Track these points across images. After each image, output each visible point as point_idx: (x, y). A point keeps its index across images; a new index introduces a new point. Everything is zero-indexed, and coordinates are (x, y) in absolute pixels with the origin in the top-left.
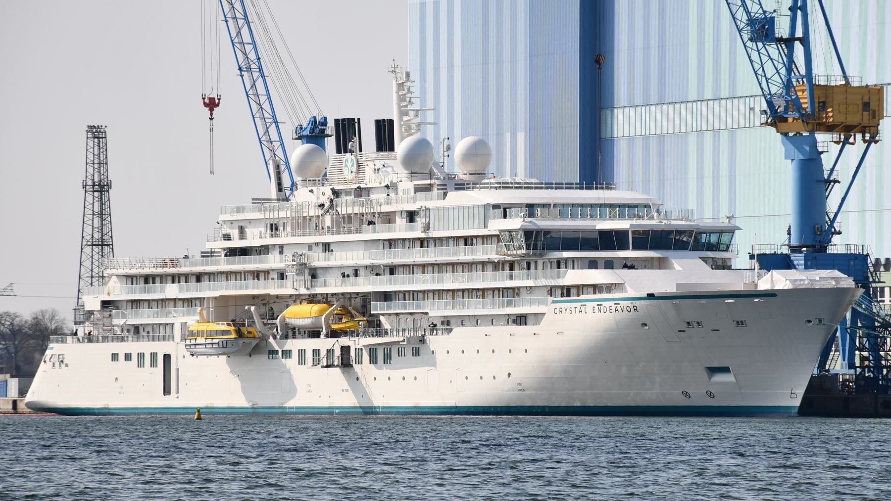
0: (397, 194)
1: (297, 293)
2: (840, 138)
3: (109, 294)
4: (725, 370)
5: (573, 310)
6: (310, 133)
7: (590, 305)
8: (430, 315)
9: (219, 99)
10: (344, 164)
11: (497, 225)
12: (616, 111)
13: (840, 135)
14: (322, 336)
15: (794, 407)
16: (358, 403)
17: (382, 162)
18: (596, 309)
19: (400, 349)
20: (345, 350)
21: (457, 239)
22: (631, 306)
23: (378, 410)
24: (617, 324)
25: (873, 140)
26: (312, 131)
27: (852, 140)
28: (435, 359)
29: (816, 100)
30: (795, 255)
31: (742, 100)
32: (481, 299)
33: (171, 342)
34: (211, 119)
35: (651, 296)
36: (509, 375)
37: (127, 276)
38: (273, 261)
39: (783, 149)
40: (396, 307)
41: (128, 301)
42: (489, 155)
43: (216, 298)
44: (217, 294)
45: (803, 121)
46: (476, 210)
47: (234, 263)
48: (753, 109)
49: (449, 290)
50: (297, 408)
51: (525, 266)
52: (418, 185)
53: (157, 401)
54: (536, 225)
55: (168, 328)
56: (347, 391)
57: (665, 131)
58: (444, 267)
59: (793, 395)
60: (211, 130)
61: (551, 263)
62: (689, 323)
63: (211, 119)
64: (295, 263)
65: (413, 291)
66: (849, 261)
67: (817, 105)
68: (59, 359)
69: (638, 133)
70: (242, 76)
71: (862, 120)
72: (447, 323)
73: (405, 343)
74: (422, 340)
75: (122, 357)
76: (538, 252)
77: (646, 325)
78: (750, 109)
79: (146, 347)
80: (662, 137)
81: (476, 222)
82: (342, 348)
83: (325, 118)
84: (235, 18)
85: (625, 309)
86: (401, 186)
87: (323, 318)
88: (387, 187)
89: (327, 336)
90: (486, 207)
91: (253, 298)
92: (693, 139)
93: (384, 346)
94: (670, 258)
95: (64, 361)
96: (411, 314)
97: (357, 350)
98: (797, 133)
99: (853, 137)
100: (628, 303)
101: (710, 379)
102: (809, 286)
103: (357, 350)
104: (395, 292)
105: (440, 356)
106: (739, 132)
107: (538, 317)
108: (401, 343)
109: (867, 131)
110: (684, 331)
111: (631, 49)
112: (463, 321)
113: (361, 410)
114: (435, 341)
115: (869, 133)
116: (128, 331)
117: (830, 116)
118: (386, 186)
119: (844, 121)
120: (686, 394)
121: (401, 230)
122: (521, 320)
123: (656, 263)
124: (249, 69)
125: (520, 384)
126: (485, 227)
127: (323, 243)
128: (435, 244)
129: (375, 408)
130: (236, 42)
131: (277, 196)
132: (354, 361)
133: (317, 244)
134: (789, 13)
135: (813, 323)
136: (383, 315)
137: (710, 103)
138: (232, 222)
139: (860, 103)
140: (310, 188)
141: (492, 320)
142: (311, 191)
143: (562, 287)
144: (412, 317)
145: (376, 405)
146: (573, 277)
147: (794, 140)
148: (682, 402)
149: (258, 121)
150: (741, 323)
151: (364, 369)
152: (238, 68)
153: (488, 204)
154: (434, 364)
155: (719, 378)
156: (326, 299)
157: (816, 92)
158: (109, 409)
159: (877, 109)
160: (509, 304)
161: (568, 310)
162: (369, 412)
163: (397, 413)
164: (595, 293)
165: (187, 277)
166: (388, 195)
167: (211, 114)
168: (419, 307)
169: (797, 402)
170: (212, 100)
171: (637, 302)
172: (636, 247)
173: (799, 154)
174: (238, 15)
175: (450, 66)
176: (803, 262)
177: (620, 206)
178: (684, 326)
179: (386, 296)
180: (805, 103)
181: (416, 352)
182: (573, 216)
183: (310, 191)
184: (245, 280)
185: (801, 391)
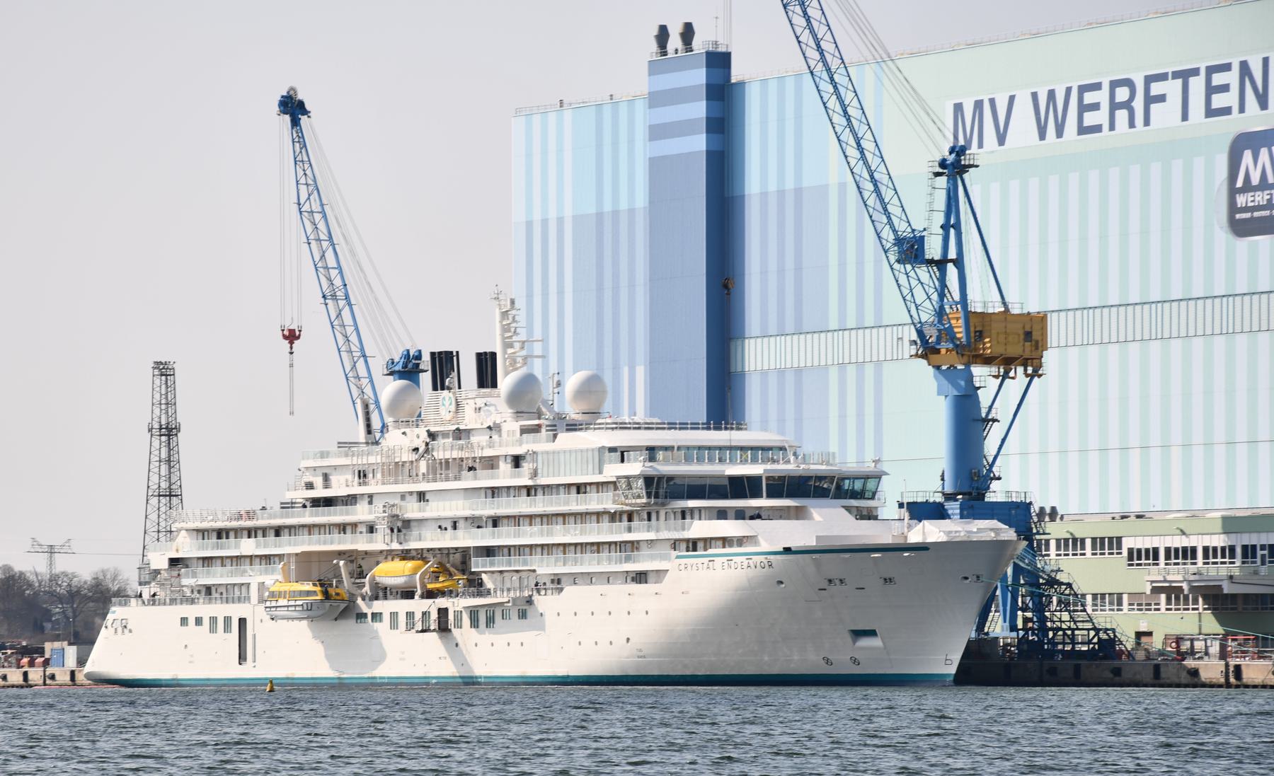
0: (500, 436)
1: (389, 548)
2: (999, 372)
4: (872, 633)
5: (700, 565)
6: (403, 368)
9: (300, 331)
11: (613, 470)
12: (747, 341)
14: (417, 597)
15: (949, 675)
16: (458, 672)
17: (484, 400)
18: (726, 564)
20: (443, 612)
22: (765, 561)
23: (479, 680)
25: (1036, 374)
26: (405, 366)
27: (1012, 374)
29: (972, 329)
30: (951, 503)
31: (889, 329)
32: (596, 554)
33: (247, 605)
35: (787, 550)
37: (198, 531)
38: (361, 513)
40: (500, 563)
42: (604, 392)
43: (297, 554)
44: (298, 550)
45: (957, 353)
46: (590, 454)
47: (317, 515)
49: (559, 544)
50: (388, 678)
51: (646, 517)
52: (524, 426)
53: (231, 670)
54: (657, 470)
55: (244, 589)
57: (802, 364)
59: (948, 662)
60: (291, 366)
61: (675, 513)
62: (830, 581)
64: (386, 515)
66: (1010, 510)
67: (972, 335)
71: (1024, 351)
72: (557, 581)
73: (510, 604)
74: (529, 601)
75: (192, 621)
76: (660, 500)
77: (782, 583)
79: (219, 610)
80: (799, 371)
81: (590, 467)
83: (420, 351)
85: (758, 564)
86: (505, 427)
87: (418, 576)
88: (489, 428)
89: (422, 597)
90: (601, 449)
91: (340, 554)
92: (834, 373)
96: (517, 571)
98: (951, 366)
99: (1013, 370)
100: (762, 558)
101: (854, 642)
104: (499, 547)
105: (549, 618)
106: (885, 364)
107: (660, 574)
108: (506, 605)
109: (1029, 364)
110: (825, 589)
111: (764, 272)
112: (575, 578)
113: (460, 680)
114: (544, 602)
115: (1032, 366)
116: (199, 592)
117: (988, 346)
119: (1003, 352)
120: (828, 661)
121: (505, 476)
122: (641, 577)
123: (793, 512)
124: (334, 297)
125: (640, 650)
126: (601, 472)
127: (417, 492)
128: (544, 493)
129: (476, 677)
130: (320, 266)
131: (366, 438)
133: (411, 493)
134: (941, 231)
136: (485, 572)
139: (1021, 332)
140: (403, 430)
141: (608, 577)
142: (404, 433)
143: (688, 541)
146: (699, 528)
147: (948, 374)
149: (344, 355)
150: (888, 580)
151: (464, 634)
152: (321, 295)
153: (603, 447)
154: (541, 627)
155: (865, 642)
156: (421, 555)
157: (973, 321)
159: (1040, 339)
160: (628, 559)
162: (470, 682)
164: (724, 547)
165: (265, 531)
166: (491, 437)
167: (291, 348)
169: (952, 670)
170: (292, 332)
171: (772, 557)
172: (771, 495)
175: (561, 292)
176: (958, 511)
177: (752, 448)
178: (825, 584)
179: (489, 552)
180: (960, 332)
181: (523, 615)
182: (700, 460)
184: (330, 534)
185: (957, 657)
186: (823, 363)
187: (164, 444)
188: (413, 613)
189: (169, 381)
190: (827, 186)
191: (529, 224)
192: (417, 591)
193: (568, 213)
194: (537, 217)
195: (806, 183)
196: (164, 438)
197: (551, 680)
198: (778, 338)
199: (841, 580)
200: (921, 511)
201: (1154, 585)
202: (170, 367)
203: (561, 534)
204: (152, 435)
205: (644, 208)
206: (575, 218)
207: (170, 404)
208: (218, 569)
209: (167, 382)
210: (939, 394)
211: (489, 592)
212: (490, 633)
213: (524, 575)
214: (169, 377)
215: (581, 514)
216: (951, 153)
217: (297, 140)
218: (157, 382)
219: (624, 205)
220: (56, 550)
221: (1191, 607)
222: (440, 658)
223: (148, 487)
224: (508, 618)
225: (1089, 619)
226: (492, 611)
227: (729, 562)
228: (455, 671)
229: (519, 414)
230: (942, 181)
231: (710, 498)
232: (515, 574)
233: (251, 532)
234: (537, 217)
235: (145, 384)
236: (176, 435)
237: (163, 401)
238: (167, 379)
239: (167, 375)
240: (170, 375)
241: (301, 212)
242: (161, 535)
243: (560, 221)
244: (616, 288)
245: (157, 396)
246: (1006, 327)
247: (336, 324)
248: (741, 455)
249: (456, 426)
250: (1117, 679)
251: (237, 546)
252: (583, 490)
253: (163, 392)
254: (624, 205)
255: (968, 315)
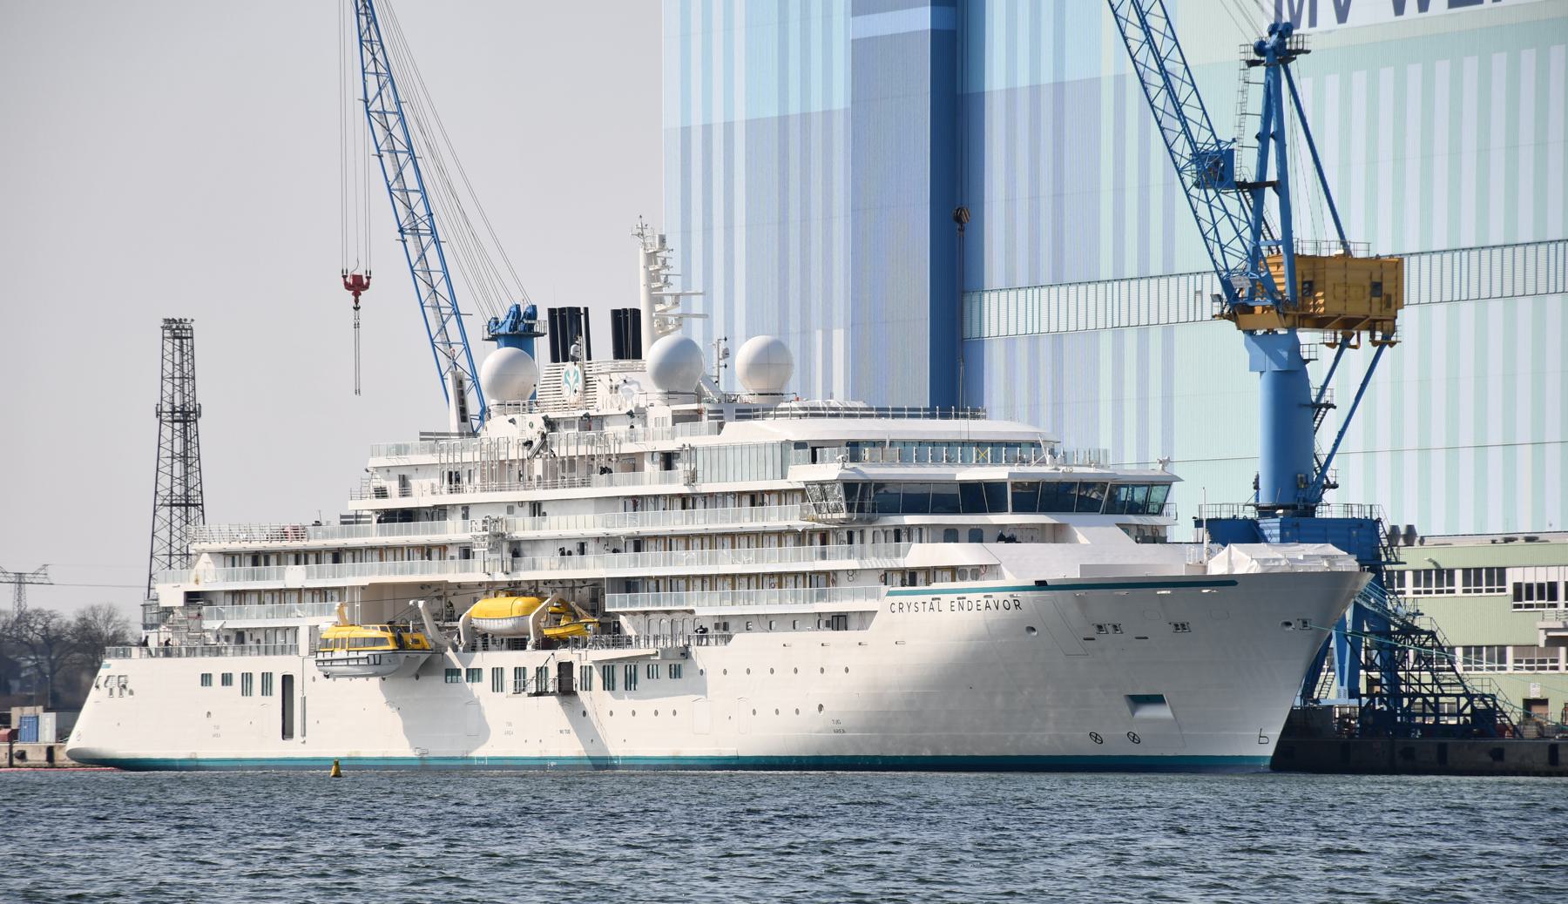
1: (490, 580)
2: (1335, 338)
3: (197, 581)
4: (1157, 700)
5: (920, 606)
6: (510, 330)
7: (946, 598)
8: (697, 613)
9: (368, 278)
10: (563, 378)
11: (801, 474)
12: (986, 295)
13: (1335, 334)
14: (529, 647)
17: (623, 376)
18: (956, 604)
19: (651, 667)
20: (565, 668)
21: (739, 495)
22: (1011, 600)
23: (616, 762)
24: (988, 627)
27: (1353, 341)
28: (705, 682)
29: (1299, 279)
31: (1183, 279)
32: (777, 589)
33: (294, 657)
34: (357, 308)
35: (1041, 585)
36: (821, 707)
37: (225, 554)
39: (1248, 355)
41: (227, 592)
43: (363, 588)
44: (365, 581)
46: (769, 450)
48: (1201, 292)
52: (678, 411)
53: (271, 747)
54: (862, 473)
56: (568, 732)
58: (720, 540)
59: (1262, 740)
60: (357, 326)
61: (886, 533)
62: (1100, 627)
63: (357, 308)
64: (487, 533)
65: (812, 573)
66: (1350, 530)
67: (1299, 287)
68: (119, 683)
69: (1022, 331)
70: (404, 241)
71: (1370, 309)
72: (724, 627)
73: (658, 658)
74: (685, 654)
75: (217, 680)
76: (865, 515)
77: (1033, 629)
78: (1196, 292)
79: (256, 664)
80: (1058, 337)
82: (560, 665)
83: (534, 307)
84: (394, 152)
85: (1001, 604)
86: (652, 414)
88: (631, 414)
89: (537, 647)
90: (785, 445)
92: (1106, 339)
93: (626, 663)
94: (1071, 525)
95: (127, 686)
96: (668, 612)
97: (495, 670)
98: (1269, 330)
99: (1355, 336)
101: (1133, 714)
102: (1287, 570)
103: (495, 670)
105: (712, 678)
106: (1178, 328)
107: (865, 617)
108: (652, 658)
110: (1093, 639)
111: (1011, 200)
112: (748, 623)
113: (589, 763)
114: (706, 656)
115: (1382, 330)
116: (227, 639)
117: (1321, 303)
118: (628, 414)
120: (1096, 737)
121: (651, 481)
122: (838, 621)
123: (1049, 532)
124: (415, 231)
126: (784, 476)
127: (530, 502)
129: (611, 759)
131: (459, 427)
132: (579, 686)
133: (521, 504)
134: (1256, 143)
135: (1293, 626)
137: (1134, 284)
138: (388, 469)
139: (1367, 283)
141: (794, 622)
142: (512, 421)
143: (903, 571)
144: (669, 618)
145: (613, 754)
146: (920, 554)
147: (1264, 341)
148: (1090, 749)
150: (1180, 627)
151: (595, 698)
152: (398, 229)
153: (788, 442)
155: (1148, 712)
156: (535, 589)
157: (1299, 268)
158: (198, 760)
159: (1393, 292)
160: (821, 597)
161: (912, 607)
162: (602, 764)
163: (646, 767)
164: (953, 580)
165: (318, 555)
166: (632, 427)
167: (357, 301)
168: (679, 601)
169: (1269, 750)
170: (358, 279)
171: (1019, 594)
172: (1018, 509)
173: (1272, 363)
174: (399, 147)
175: (729, 227)
177: (992, 444)
178: (1093, 632)
179: (629, 585)
180: (1282, 283)
181: (676, 672)
182: (921, 460)
183: (510, 421)
185: (1275, 733)
186: (1091, 326)
187: (178, 433)
188: (210, 675)
189: (185, 347)
190: (1098, 80)
191: (686, 131)
192: (529, 639)
193: (740, 116)
194: (697, 122)
195: (1070, 75)
196: (177, 426)
197: (716, 763)
198: (1030, 291)
199: (1115, 626)
200: (1225, 531)
201: (1550, 634)
202: (187, 326)
203: (728, 562)
204: (161, 421)
205: (846, 109)
206: (751, 125)
207: (186, 377)
208: (253, 607)
209: (181, 347)
210: (1251, 369)
211: (629, 642)
212: (630, 698)
213: (677, 617)
214: (185, 341)
215: (756, 534)
216: (1271, 34)
217: (362, 11)
218: (169, 347)
219: (817, 106)
220: (27, 580)
221: (1485, 666)
222: (561, 732)
223: (156, 492)
224: (655, 677)
225: (1458, 681)
226: (655, 667)
227: (961, 601)
228: (582, 749)
229: (671, 395)
230: (1259, 73)
231: (934, 512)
232: (665, 615)
233: (300, 557)
234: (697, 122)
235: (152, 346)
236: (195, 421)
237: (177, 374)
238: (182, 343)
239: (181, 338)
240: (187, 338)
241: (368, 113)
242: (175, 461)
243: (729, 127)
244: (805, 220)
245: (169, 367)
246: (1345, 276)
247: (417, 270)
248: (978, 453)
249: (584, 412)
250: (1498, 765)
251: (280, 576)
252: (759, 500)
253: (177, 361)
254: (817, 106)
255: (1294, 259)
